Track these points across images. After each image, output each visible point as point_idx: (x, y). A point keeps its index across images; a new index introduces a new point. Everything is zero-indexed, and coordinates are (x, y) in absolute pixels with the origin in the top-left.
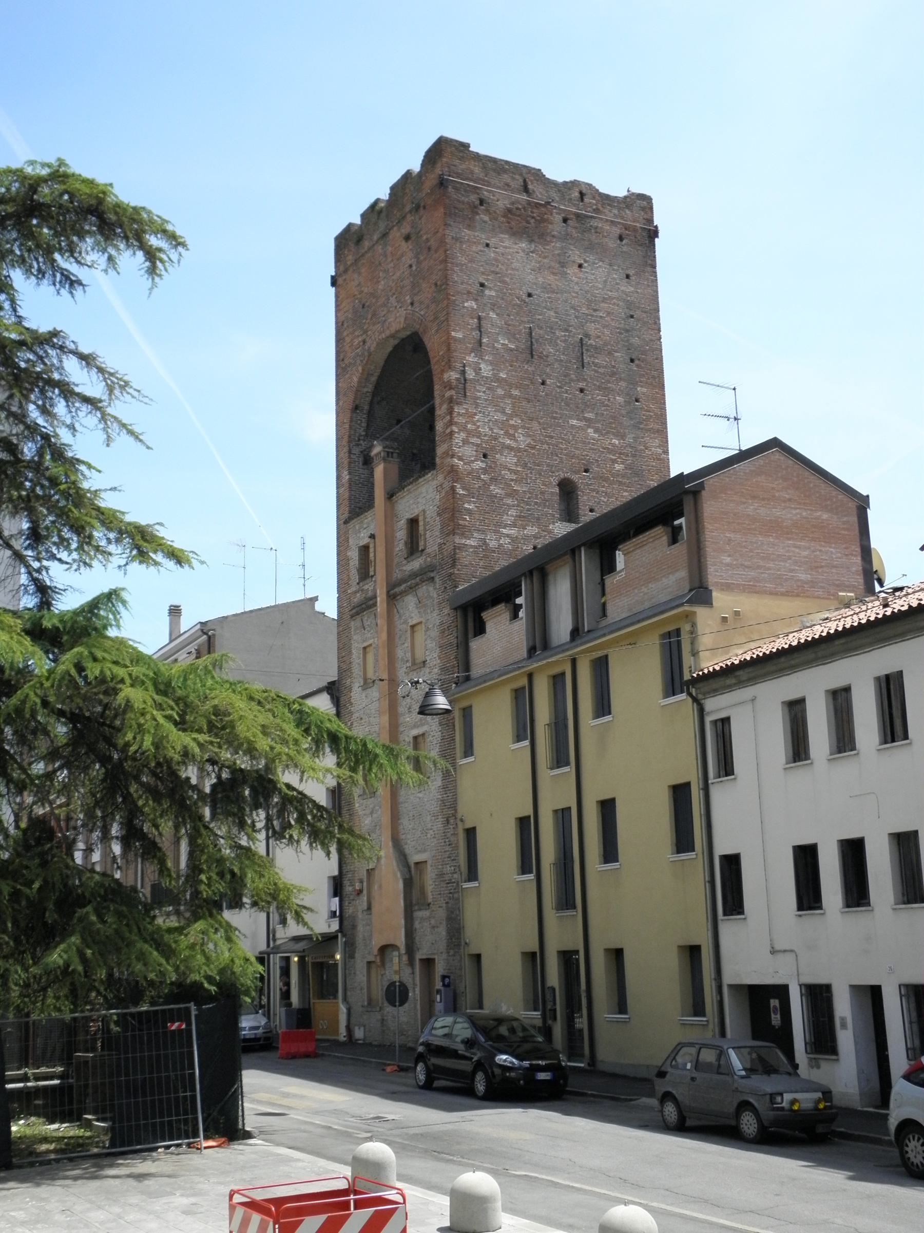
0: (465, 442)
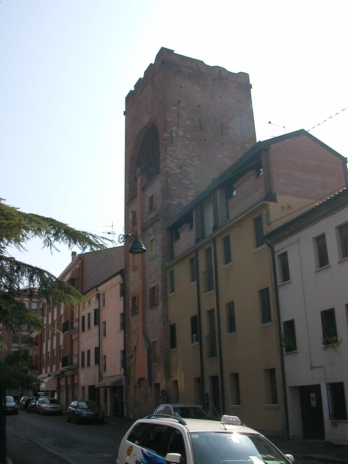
0: (172, 161)
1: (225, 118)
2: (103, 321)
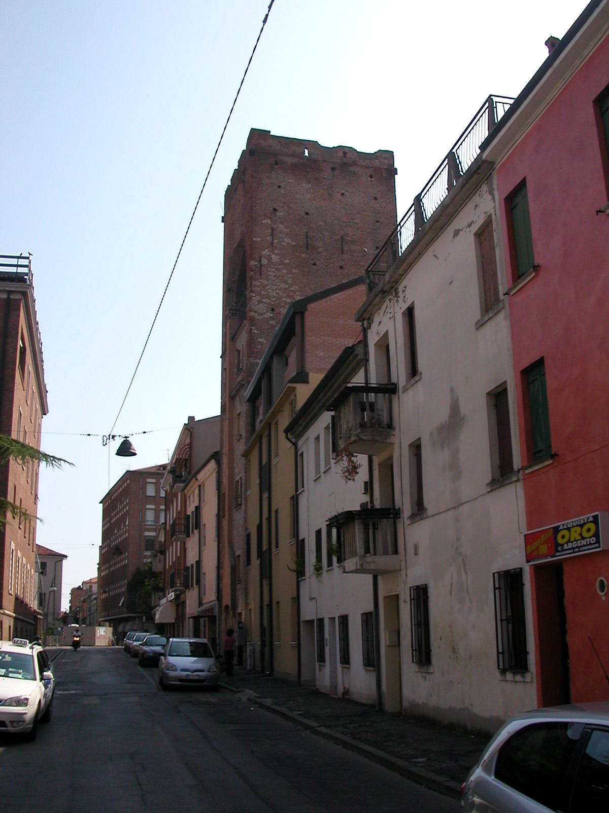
1: (349, 227)
2: (204, 523)
